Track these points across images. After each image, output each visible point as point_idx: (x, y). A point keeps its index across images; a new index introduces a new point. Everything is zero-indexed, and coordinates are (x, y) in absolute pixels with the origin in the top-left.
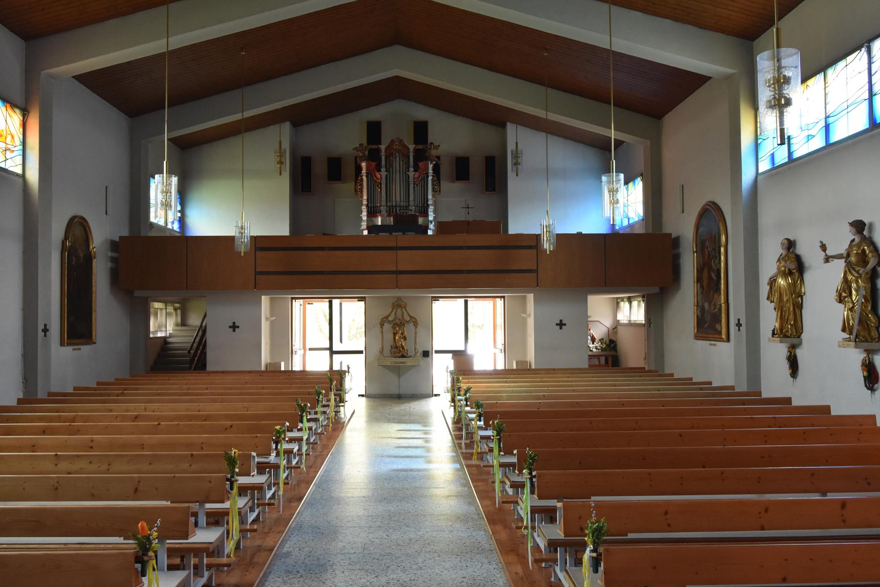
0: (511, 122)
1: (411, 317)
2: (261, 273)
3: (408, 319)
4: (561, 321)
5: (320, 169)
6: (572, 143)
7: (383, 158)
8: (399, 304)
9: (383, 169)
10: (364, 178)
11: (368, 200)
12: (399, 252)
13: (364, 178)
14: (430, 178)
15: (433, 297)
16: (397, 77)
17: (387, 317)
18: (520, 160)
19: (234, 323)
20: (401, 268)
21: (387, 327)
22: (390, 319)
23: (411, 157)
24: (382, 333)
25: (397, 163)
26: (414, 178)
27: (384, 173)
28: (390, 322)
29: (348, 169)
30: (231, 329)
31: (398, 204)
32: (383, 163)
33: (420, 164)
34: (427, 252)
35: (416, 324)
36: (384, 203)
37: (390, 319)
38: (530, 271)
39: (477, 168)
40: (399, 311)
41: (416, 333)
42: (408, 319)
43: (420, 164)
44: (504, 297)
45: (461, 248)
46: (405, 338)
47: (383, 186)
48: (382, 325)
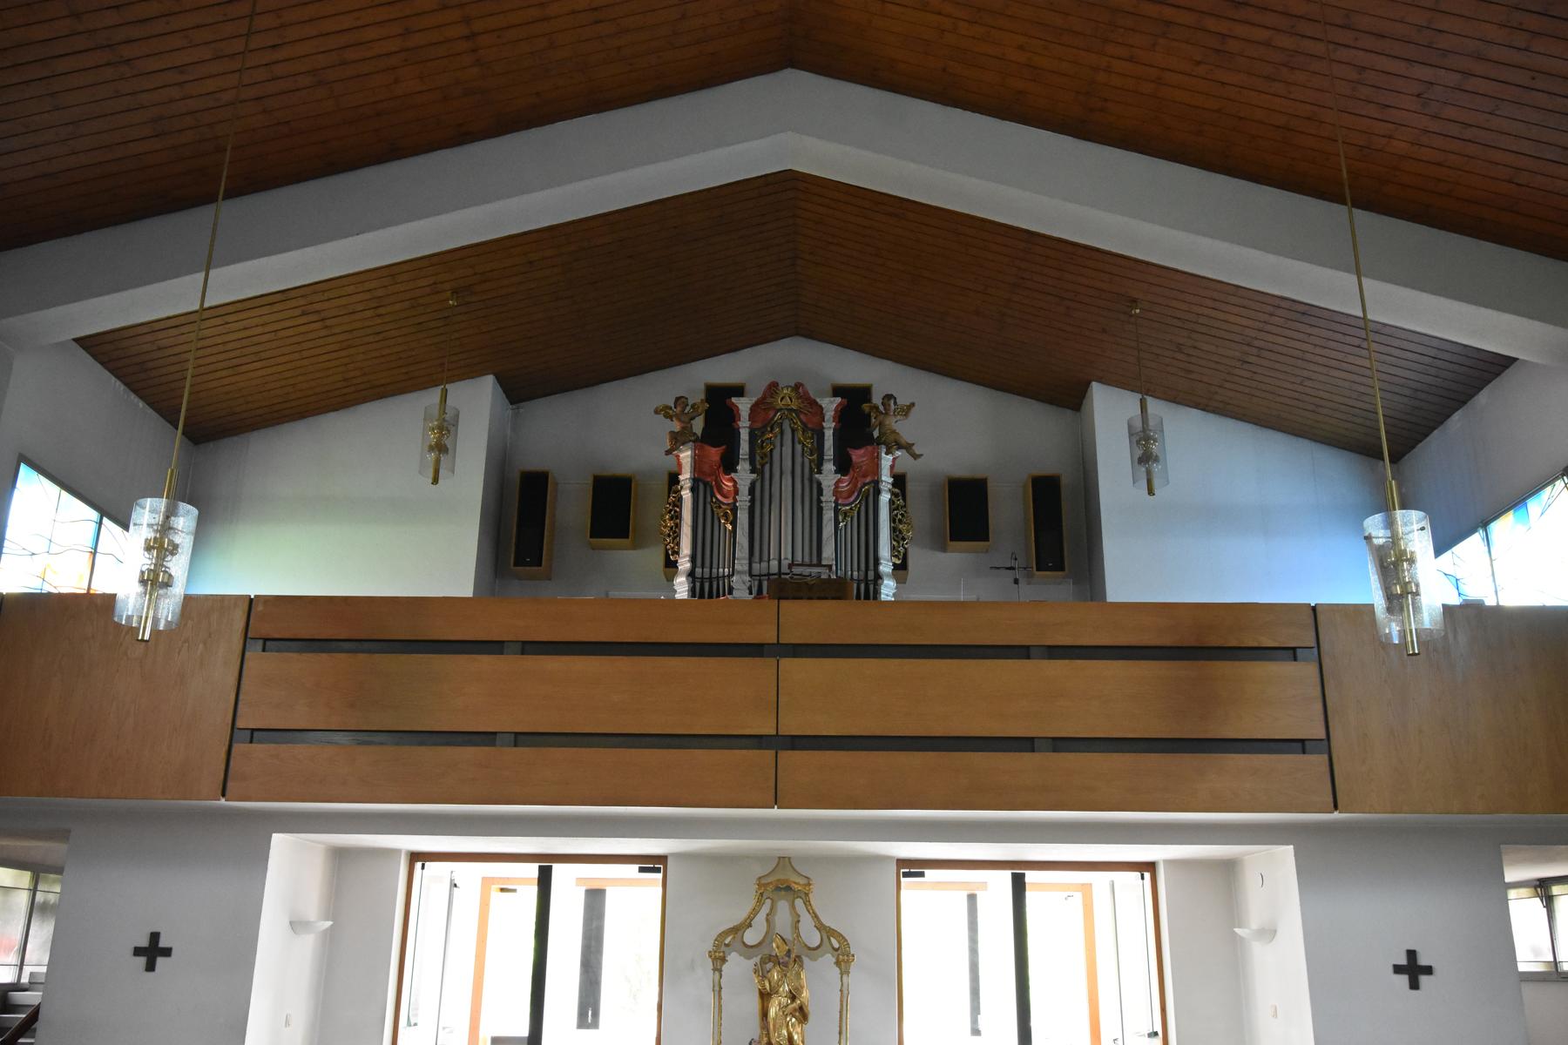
0: (1100, 380)
1: (827, 932)
2: (253, 734)
3: (814, 938)
4: (150, 967)
5: (571, 508)
6: (1279, 436)
7: (744, 435)
8: (782, 883)
9: (743, 467)
10: (686, 495)
11: (693, 559)
12: (786, 663)
13: (686, 495)
14: (885, 497)
15: (902, 863)
16: (788, 180)
17: (737, 930)
18: (1155, 448)
19: (155, 937)
20: (792, 725)
21: (738, 967)
22: (751, 937)
23: (829, 435)
24: (718, 990)
25: (785, 452)
26: (836, 493)
27: (744, 475)
28: (748, 950)
29: (648, 511)
30: (161, 962)
31: (785, 569)
32: (744, 448)
33: (858, 456)
34: (893, 665)
35: (844, 959)
36: (741, 564)
37: (751, 937)
38: (1301, 745)
39: (1009, 511)
40: (783, 906)
41: (843, 994)
42: (814, 938)
43: (858, 456)
44: (1150, 867)
45: (1022, 652)
46: (802, 1014)
47: (743, 517)
48: (719, 960)
